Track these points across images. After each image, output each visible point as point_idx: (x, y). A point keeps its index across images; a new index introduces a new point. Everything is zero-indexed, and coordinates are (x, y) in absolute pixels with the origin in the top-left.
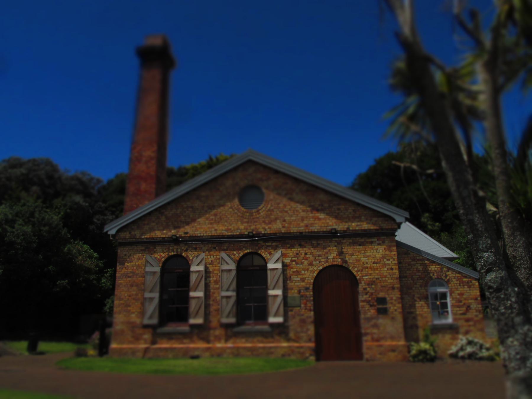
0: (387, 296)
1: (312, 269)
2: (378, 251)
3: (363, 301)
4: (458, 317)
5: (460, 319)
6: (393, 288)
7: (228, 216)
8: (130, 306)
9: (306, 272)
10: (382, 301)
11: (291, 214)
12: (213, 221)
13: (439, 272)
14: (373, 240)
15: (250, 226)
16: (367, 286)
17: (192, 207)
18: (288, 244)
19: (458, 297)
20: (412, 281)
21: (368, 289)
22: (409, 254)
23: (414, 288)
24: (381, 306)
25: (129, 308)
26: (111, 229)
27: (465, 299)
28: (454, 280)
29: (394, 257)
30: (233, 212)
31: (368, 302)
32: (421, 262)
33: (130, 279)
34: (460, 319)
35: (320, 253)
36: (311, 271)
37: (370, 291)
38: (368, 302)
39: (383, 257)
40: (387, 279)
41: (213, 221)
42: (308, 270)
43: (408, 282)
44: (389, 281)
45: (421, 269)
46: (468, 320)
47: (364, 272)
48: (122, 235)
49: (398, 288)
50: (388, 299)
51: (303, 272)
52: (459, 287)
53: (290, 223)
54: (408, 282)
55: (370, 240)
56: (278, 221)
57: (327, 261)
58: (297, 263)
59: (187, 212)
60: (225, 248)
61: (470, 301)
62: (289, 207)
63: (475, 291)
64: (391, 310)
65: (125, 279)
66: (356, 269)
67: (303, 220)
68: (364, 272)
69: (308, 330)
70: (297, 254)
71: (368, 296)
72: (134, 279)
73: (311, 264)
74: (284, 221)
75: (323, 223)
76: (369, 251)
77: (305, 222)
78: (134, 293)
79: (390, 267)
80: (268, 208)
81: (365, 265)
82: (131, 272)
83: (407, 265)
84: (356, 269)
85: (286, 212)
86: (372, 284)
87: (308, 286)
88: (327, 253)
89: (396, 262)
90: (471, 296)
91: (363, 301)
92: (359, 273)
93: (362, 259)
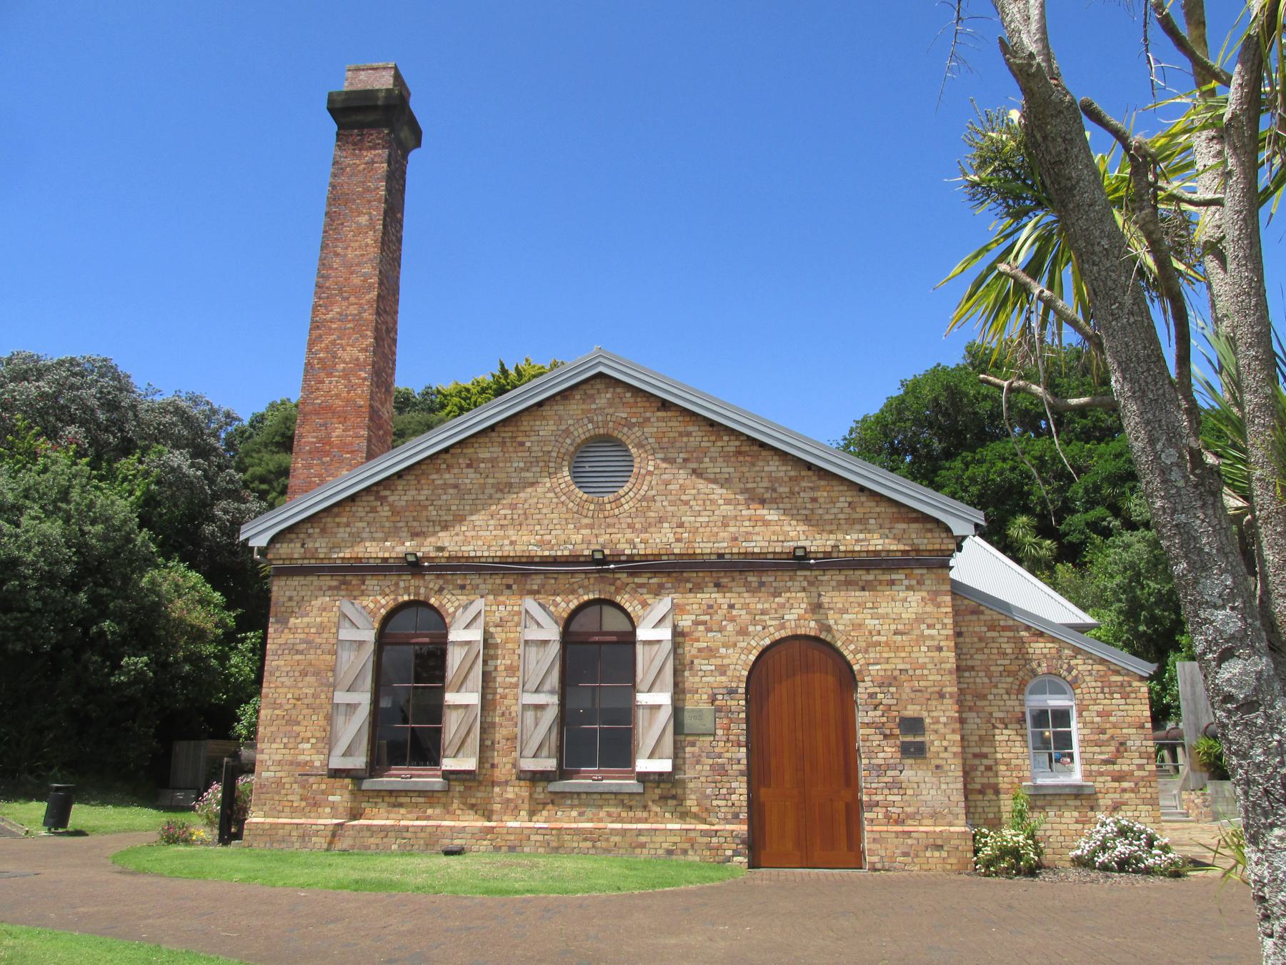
0: (925, 714)
1: (744, 645)
2: (906, 605)
3: (868, 725)
6: (942, 696)
7: (544, 511)
10: (913, 725)
11: (697, 508)
12: (505, 522)
14: (894, 577)
16: (878, 690)
17: (456, 486)
18: (688, 581)
19: (1097, 719)
20: (986, 680)
21: (880, 696)
22: (982, 613)
28: (1088, 679)
29: (946, 621)
30: (555, 500)
31: (879, 727)
32: (1011, 634)
34: (1101, 774)
36: (743, 649)
37: (884, 702)
38: (879, 727)
39: (919, 619)
40: (926, 672)
42: (735, 645)
46: (1118, 778)
47: (872, 655)
48: (283, 549)
50: (928, 721)
52: (1101, 696)
54: (978, 680)
55: (888, 577)
57: (783, 627)
58: (709, 630)
59: (444, 497)
60: (535, 587)
61: (1125, 731)
62: (694, 492)
65: (289, 658)
66: (852, 647)
67: (725, 525)
68: (872, 655)
69: (731, 791)
70: (710, 607)
73: (743, 632)
74: (681, 525)
76: (884, 605)
77: (732, 529)
79: (936, 643)
80: (642, 492)
84: (852, 647)
85: (687, 503)
86: (890, 685)
87: (734, 685)
91: (868, 725)
92: (859, 656)
93: (867, 622)
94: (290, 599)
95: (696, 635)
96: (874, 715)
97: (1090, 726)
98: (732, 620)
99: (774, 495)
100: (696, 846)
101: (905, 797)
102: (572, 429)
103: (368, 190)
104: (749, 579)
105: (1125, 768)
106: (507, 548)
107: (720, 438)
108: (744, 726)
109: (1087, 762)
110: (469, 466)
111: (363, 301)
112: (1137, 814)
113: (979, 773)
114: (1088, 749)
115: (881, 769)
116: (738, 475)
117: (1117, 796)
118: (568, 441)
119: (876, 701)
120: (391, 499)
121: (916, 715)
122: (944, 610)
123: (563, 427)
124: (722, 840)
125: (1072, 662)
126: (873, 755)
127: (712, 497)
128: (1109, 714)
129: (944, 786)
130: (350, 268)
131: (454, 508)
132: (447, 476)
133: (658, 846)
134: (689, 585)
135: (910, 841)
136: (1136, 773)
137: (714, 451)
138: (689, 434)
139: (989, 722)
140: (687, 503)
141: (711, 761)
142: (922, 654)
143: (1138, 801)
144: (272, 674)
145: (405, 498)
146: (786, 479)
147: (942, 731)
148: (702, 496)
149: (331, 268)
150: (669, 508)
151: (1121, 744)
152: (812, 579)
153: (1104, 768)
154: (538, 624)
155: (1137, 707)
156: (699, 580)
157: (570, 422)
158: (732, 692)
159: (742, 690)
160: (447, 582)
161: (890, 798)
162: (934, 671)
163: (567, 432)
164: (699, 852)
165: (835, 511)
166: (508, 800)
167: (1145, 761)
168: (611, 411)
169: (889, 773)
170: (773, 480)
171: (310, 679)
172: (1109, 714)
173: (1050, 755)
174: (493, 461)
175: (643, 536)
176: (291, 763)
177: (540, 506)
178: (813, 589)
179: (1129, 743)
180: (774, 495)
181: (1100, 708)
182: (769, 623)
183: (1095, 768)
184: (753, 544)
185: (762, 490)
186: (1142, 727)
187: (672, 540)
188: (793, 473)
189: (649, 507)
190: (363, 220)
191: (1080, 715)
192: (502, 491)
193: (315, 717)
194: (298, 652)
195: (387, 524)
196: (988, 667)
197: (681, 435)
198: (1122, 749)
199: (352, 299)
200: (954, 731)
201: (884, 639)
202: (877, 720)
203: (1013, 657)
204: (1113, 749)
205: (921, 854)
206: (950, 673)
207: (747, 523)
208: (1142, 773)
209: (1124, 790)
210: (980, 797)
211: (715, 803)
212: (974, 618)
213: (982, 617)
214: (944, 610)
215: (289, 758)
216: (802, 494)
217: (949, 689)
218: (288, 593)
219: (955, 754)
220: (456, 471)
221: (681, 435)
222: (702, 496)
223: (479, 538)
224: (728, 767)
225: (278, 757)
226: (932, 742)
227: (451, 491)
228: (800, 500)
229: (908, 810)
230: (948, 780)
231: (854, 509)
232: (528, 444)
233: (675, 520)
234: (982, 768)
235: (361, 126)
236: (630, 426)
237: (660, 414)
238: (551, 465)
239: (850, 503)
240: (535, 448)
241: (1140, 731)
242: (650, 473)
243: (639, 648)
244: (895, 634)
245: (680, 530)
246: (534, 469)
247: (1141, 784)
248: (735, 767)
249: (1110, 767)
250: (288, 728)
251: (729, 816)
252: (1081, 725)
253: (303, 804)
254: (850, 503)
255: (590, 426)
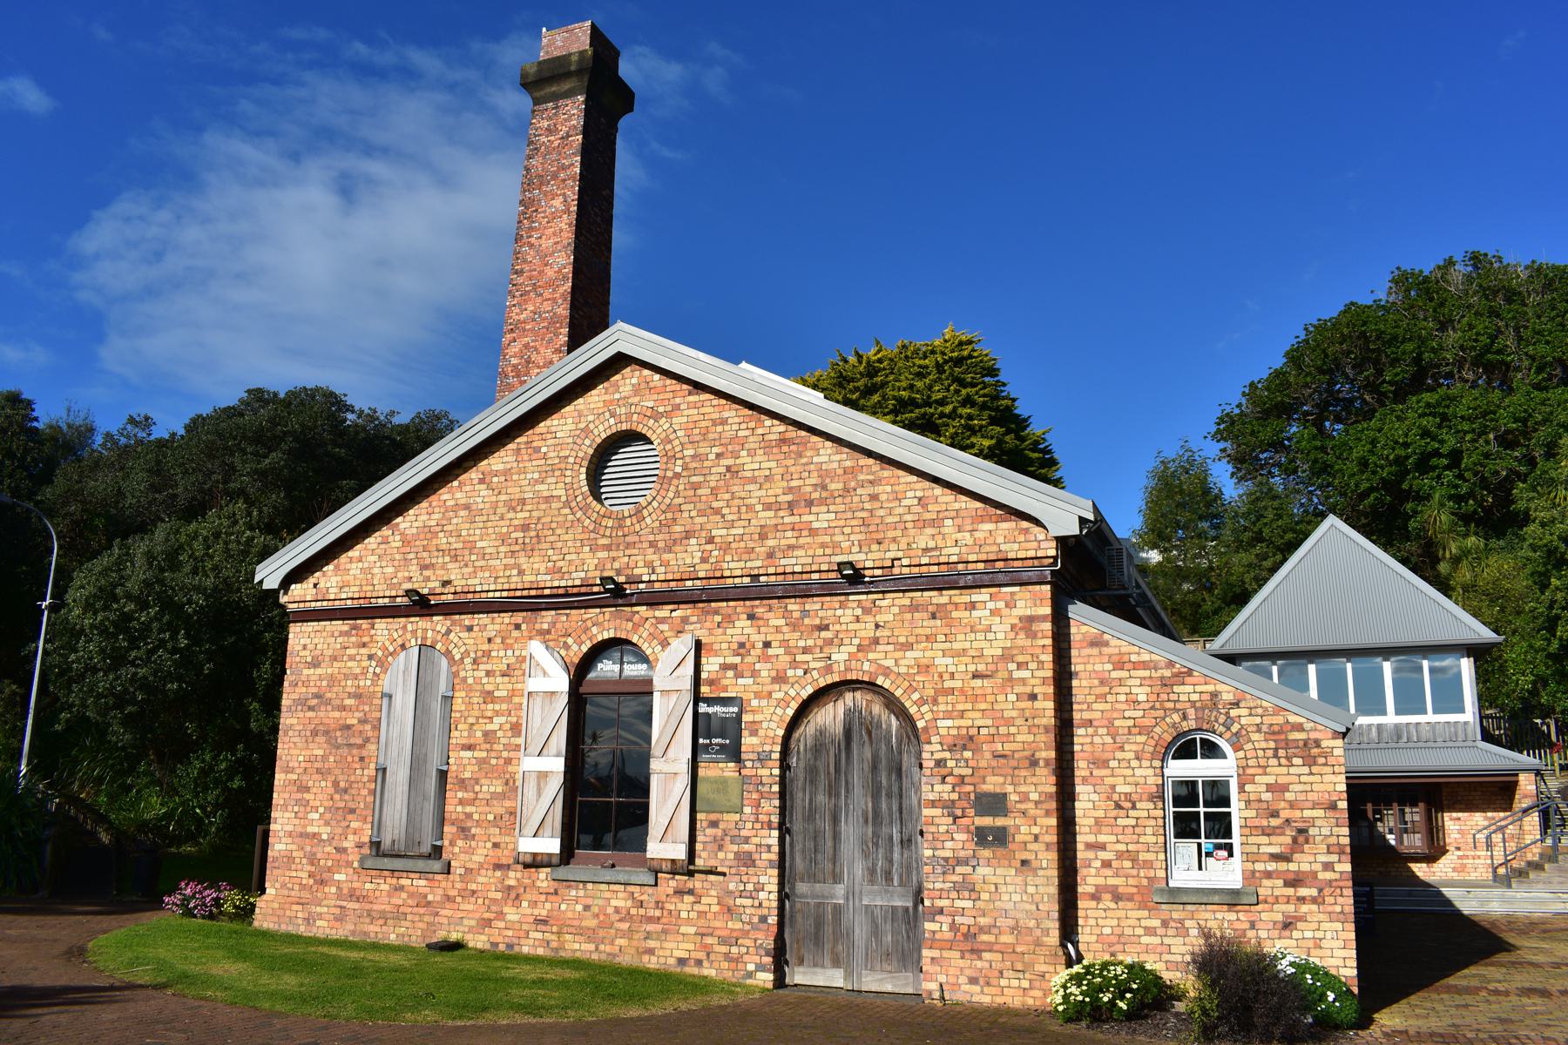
0: (1010, 789)
1: (780, 695)
2: (990, 636)
3: (933, 804)
4: (1259, 867)
5: (1268, 875)
6: (1034, 763)
7: (558, 531)
8: (307, 789)
9: (764, 702)
10: (994, 804)
11: (730, 517)
12: (517, 548)
13: (1203, 709)
14: (975, 598)
15: (614, 559)
16: (947, 755)
17: (467, 507)
18: (716, 612)
19: (1267, 796)
20: (1108, 740)
21: (950, 764)
22: (1107, 644)
23: (1113, 764)
24: (987, 821)
25: (307, 796)
26: (269, 574)
27: (1292, 805)
28: (1255, 737)
29: (1043, 658)
30: (570, 517)
31: (949, 806)
32: (1146, 673)
33: (311, 714)
34: (1268, 875)
35: (810, 643)
36: (779, 701)
37: (956, 771)
38: (949, 806)
39: (1007, 656)
40: (1013, 730)
41: (517, 548)
42: (770, 694)
43: (1097, 740)
44: (1019, 738)
45: (1142, 698)
46: (1294, 881)
47: (942, 707)
48: (297, 590)
49: (1047, 761)
50: (1014, 797)
51: (755, 703)
52: (1273, 762)
53: (726, 548)
54: (1097, 740)
55: (966, 599)
56: (693, 541)
57: (828, 669)
58: (739, 675)
59: (455, 521)
60: (545, 626)
61: (1307, 813)
62: (727, 496)
63: (1328, 778)
64: (1018, 838)
65: (301, 715)
66: (916, 696)
67: (763, 537)
68: (942, 707)
69: (759, 888)
70: (742, 645)
71: (948, 788)
72: (321, 714)
73: (780, 679)
74: (711, 540)
75: (823, 546)
76: (960, 637)
77: (771, 543)
78: (320, 752)
79: (1028, 690)
80: (667, 501)
81: (948, 684)
82: (316, 696)
83: (1096, 682)
84: (916, 696)
85: (717, 511)
86: (965, 748)
87: (767, 748)
88: (829, 642)
89: (1050, 674)
90: (1311, 796)
91: (933, 804)
92: (925, 709)
93: (937, 661)
94: (305, 647)
95: (725, 682)
96: (944, 791)
97: (1254, 805)
99: (824, 494)
100: (712, 957)
101: (978, 904)
102: (591, 426)
103: (564, 168)
104: (790, 607)
105: (1305, 867)
106: (514, 579)
107: (761, 423)
108: (777, 803)
109: (1249, 857)
110: (482, 481)
112: (1319, 935)
113: (1093, 871)
114: (1252, 840)
115: (950, 864)
116: (781, 470)
117: (1291, 908)
118: (587, 442)
119: (944, 771)
120: (402, 526)
121: (998, 790)
122: (1041, 642)
123: (582, 426)
124: (744, 950)
125: (1233, 713)
126: (939, 845)
127: (748, 501)
128: (1284, 788)
129: (1031, 890)
130: (544, 257)
131: (464, 533)
132: (458, 495)
133: (668, 953)
134: (718, 618)
135: (979, 964)
136: (1321, 876)
137: (753, 442)
138: (724, 422)
139: (1109, 799)
141: (735, 848)
142: (1009, 703)
143: (1322, 917)
144: (286, 734)
145: (416, 524)
146: (840, 471)
147: (1032, 812)
148: (737, 502)
149: (525, 261)
150: (699, 520)
151: (1301, 831)
152: (868, 605)
153: (1271, 866)
154: (545, 673)
155: (1328, 778)
156: (730, 611)
157: (591, 418)
159: (776, 756)
160: (454, 623)
161: (959, 903)
162: (1025, 729)
163: (586, 431)
164: (716, 965)
165: (901, 510)
166: (510, 888)
167: (1335, 858)
168: (636, 400)
169: (959, 869)
170: (824, 474)
171: (321, 739)
172: (1284, 788)
173: (1199, 845)
174: (507, 473)
175: (666, 556)
176: (301, 835)
177: (554, 525)
178: (868, 618)
179: (1312, 831)
180: (824, 494)
181: (1271, 780)
182: (812, 665)
183: (1259, 867)
184: (793, 561)
185: (809, 489)
186: (1333, 806)
187: (697, 560)
188: (848, 464)
189: (674, 520)
191: (1241, 789)
192: (514, 509)
193: (323, 784)
194: (311, 708)
195: (397, 557)
196: (1111, 722)
197: (715, 423)
198: (1301, 839)
200: (1048, 813)
201: (958, 684)
202: (946, 796)
203: (1147, 706)
204: (1288, 840)
205: (994, 981)
206: (1047, 730)
207: (789, 534)
208: (1329, 875)
209: (1302, 900)
210: (1093, 904)
211: (739, 902)
212: (1095, 651)
213: (1106, 650)
214: (1041, 642)
215: (299, 829)
216: (859, 491)
217: (1044, 754)
218: (303, 641)
219: (1048, 845)
220: (468, 488)
221: (715, 423)
222: (737, 502)
223: (488, 568)
224: (756, 856)
225: (290, 828)
226: (1018, 827)
227: (462, 513)
228: (856, 499)
229: (982, 921)
230: (1038, 881)
231: (924, 506)
232: (544, 450)
233: (704, 534)
234: (1098, 864)
235: (555, 97)
237: (691, 398)
238: (568, 473)
239: (920, 499)
240: (552, 454)
241: (1330, 814)
242: (677, 476)
243: (656, 696)
244: (975, 677)
245: (709, 547)
246: (549, 480)
247: (1327, 891)
248: (764, 856)
249: (1283, 866)
250: (299, 796)
251: (756, 920)
252: (1243, 805)
253: (311, 881)
254: (920, 499)
255: (612, 421)
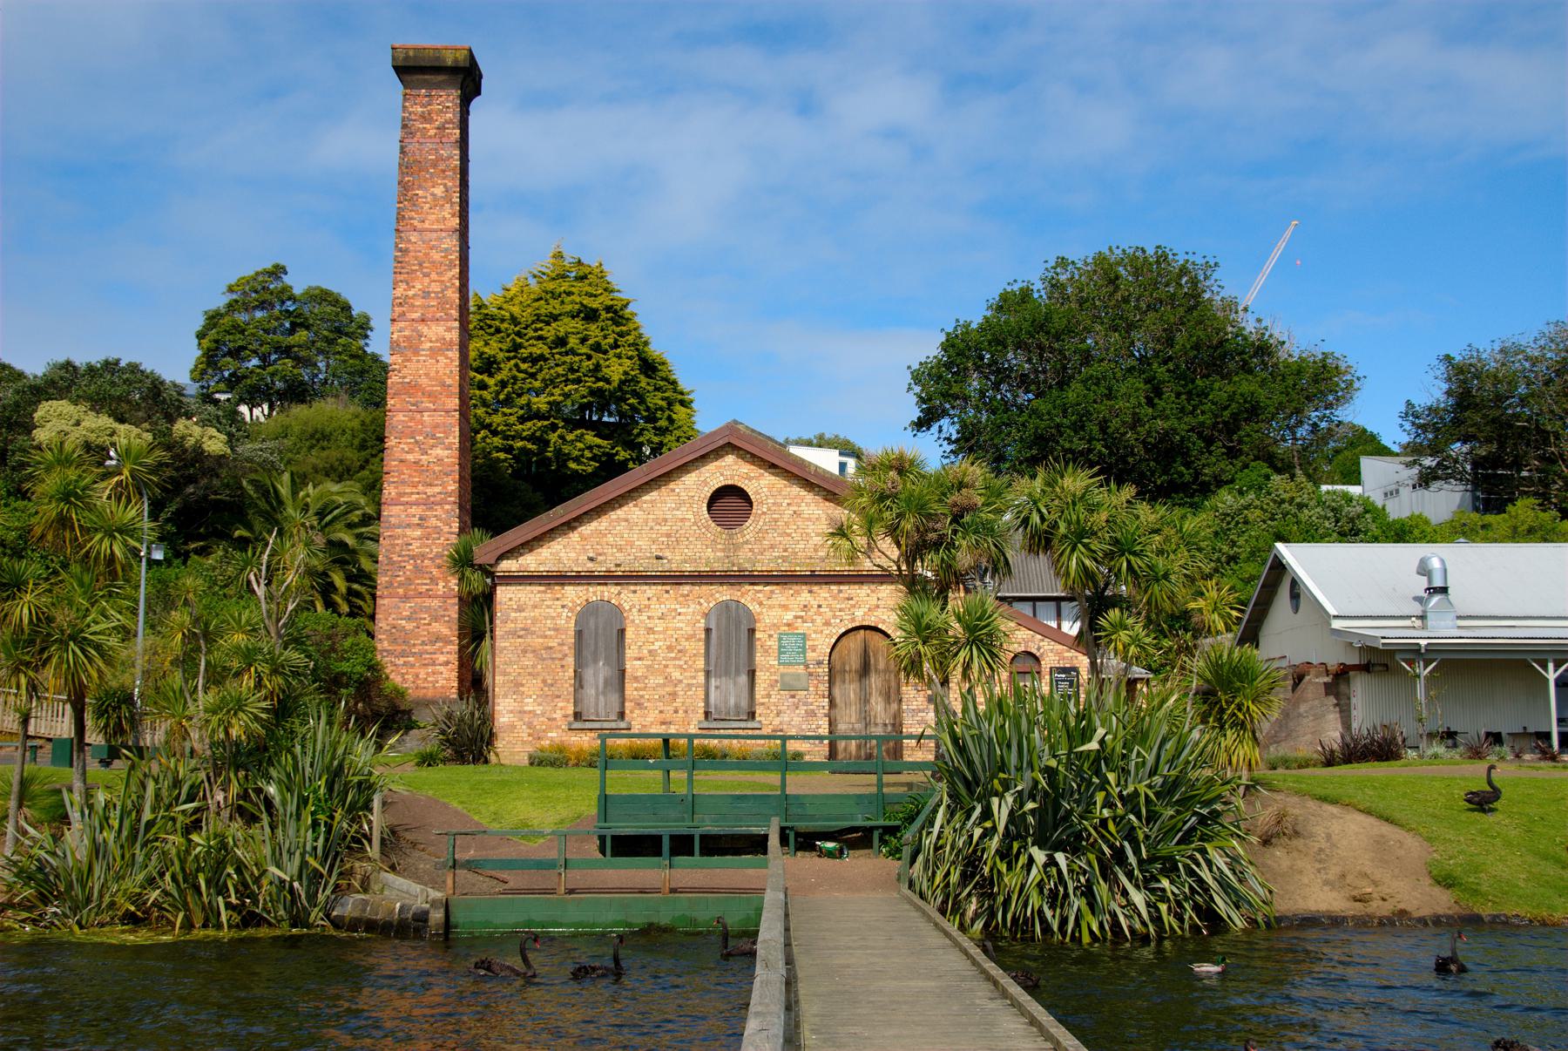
73: (827, 624)
98: (820, 614)
111: (445, 278)
140: (789, 535)
158: (819, 663)
190: (439, 191)
199: (434, 276)
236: (750, 479)
